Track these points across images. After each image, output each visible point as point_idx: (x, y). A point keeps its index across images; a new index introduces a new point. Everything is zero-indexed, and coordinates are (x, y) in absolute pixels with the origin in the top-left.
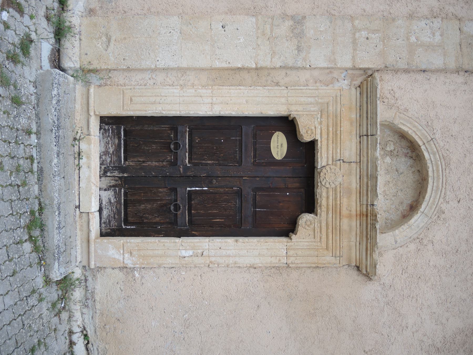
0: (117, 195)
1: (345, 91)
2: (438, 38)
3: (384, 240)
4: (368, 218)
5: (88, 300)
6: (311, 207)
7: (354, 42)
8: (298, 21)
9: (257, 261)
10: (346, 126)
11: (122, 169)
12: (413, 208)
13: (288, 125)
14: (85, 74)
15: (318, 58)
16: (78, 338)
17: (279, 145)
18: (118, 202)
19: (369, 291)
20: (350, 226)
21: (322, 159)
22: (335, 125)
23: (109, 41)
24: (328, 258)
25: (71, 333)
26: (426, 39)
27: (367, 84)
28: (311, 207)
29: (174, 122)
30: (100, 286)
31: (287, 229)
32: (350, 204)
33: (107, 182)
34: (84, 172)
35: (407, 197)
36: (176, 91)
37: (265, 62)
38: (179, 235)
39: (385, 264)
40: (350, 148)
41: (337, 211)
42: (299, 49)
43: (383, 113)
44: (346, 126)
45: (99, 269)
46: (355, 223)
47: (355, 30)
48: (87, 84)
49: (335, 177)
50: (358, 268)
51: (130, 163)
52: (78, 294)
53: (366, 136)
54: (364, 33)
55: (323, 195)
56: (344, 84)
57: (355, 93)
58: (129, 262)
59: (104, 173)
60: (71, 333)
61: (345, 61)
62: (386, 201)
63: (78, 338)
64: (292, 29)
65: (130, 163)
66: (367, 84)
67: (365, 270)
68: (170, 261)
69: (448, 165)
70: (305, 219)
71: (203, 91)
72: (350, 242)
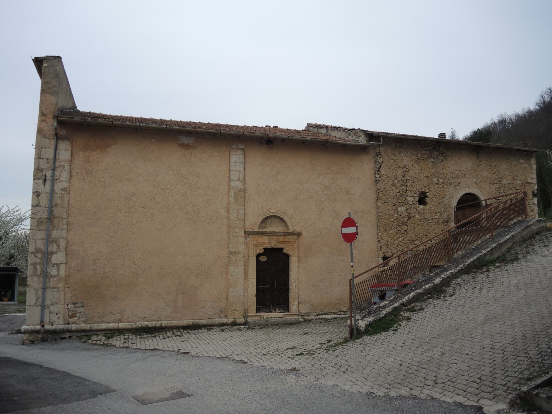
0: (277, 308)
1: (250, 239)
2: (235, 211)
3: (291, 229)
4: (285, 234)
5: (307, 314)
6: (281, 249)
7: (237, 237)
8: (231, 253)
9: (297, 265)
10: (259, 239)
11: (270, 306)
12: (281, 219)
13: (258, 256)
14: (245, 317)
15: (242, 247)
16: (318, 317)
17: (263, 259)
18: (279, 307)
19: (305, 233)
20: (287, 239)
21: (269, 246)
22: (259, 242)
23: (236, 310)
24: (296, 245)
25: (316, 319)
26: (236, 215)
27: (248, 233)
28: (281, 249)
29: (258, 290)
30: (303, 311)
31: (287, 256)
32: (281, 239)
33: (273, 311)
34: (272, 316)
35: (278, 221)
36: (249, 289)
37: (242, 263)
38: (289, 289)
39: (298, 229)
40: (266, 238)
41: (283, 242)
42: (239, 253)
43: (256, 229)
44: (259, 239)
45: (299, 312)
46: (286, 237)
47: (233, 236)
48: (248, 316)
49: (274, 243)
50: (298, 237)
51: (268, 304)
52: (306, 317)
53: (263, 234)
54: (234, 234)
55: (279, 246)
56: (248, 239)
57: (250, 237)
58: (297, 303)
59: (271, 312)
60: (316, 319)
61: (242, 240)
62: (278, 228)
63: (318, 317)
64: (233, 255)
65: (268, 304)
66: (248, 233)
67: (299, 235)
68: (297, 291)
69: (270, 209)
70: (285, 251)
71: (250, 281)
72: (292, 239)
